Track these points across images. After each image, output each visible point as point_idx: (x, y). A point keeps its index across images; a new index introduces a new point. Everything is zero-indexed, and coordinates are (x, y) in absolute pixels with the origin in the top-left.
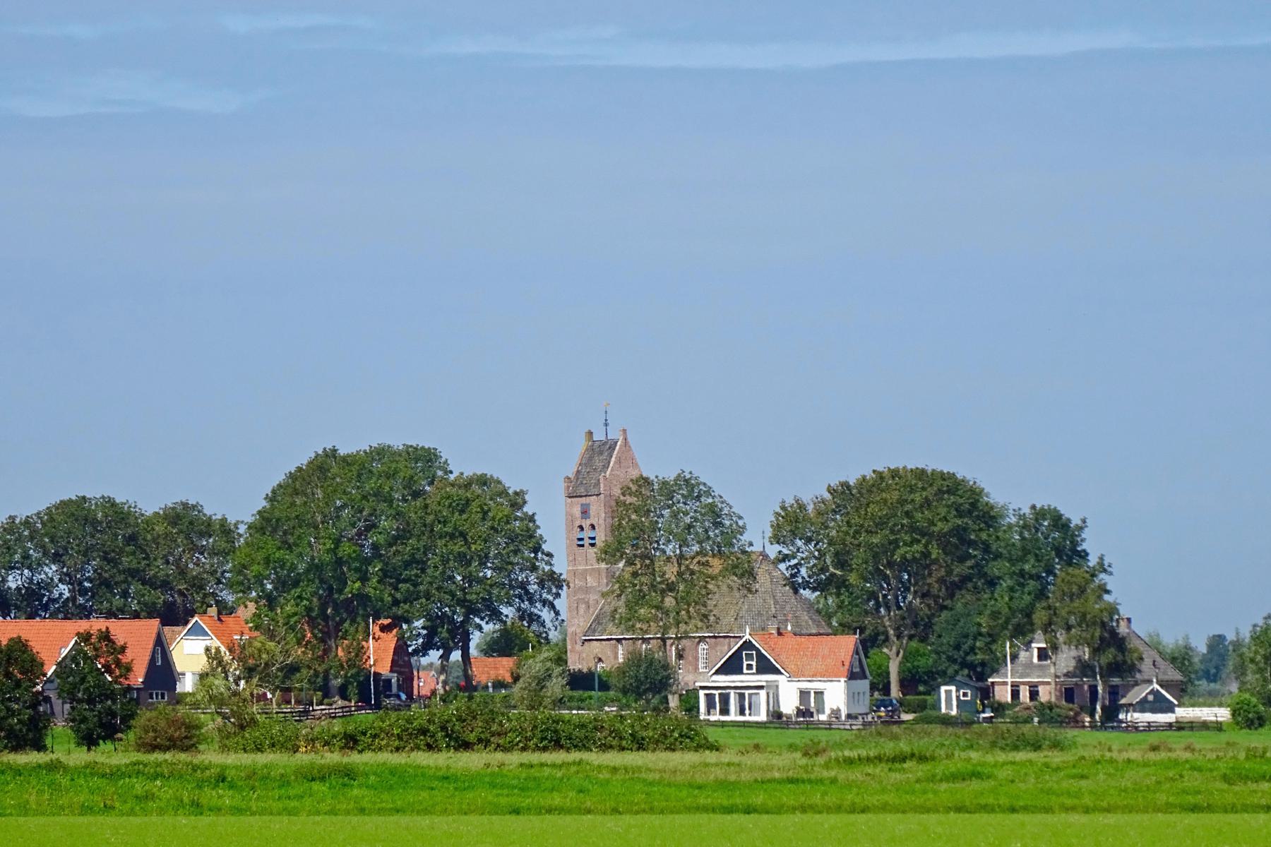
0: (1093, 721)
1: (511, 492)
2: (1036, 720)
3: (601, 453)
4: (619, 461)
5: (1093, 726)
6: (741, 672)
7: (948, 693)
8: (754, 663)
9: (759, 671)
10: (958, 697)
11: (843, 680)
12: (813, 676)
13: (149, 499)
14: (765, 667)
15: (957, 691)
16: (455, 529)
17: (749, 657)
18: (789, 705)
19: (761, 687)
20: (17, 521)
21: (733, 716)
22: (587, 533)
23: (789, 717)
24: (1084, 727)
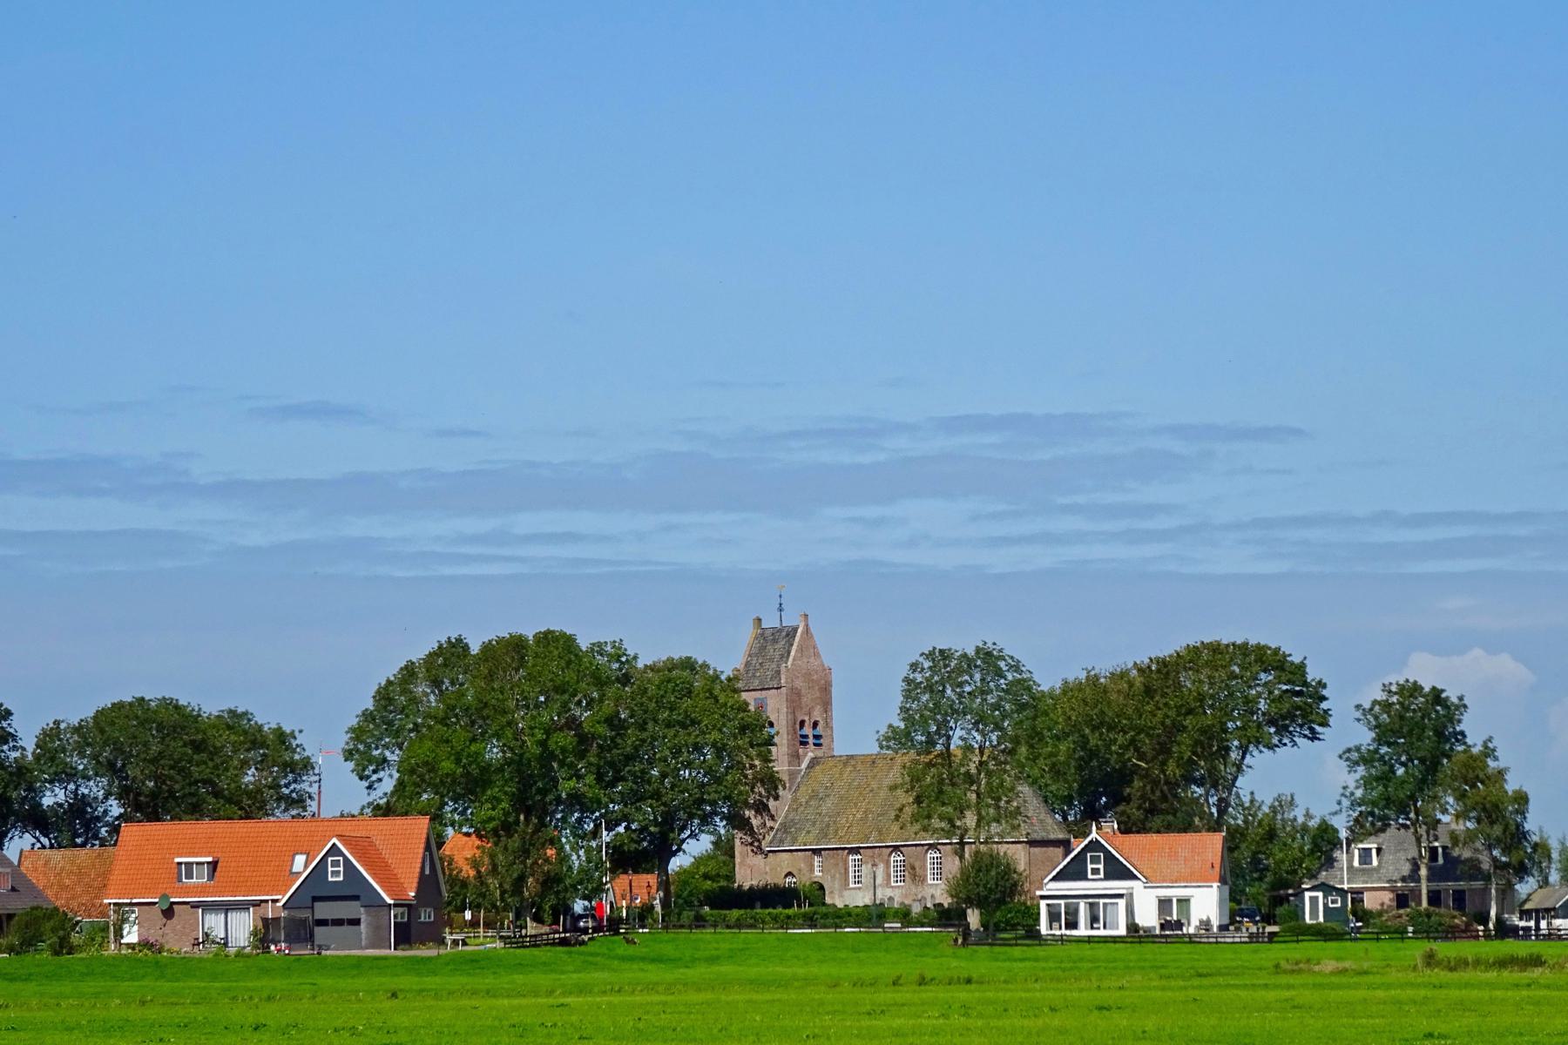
0: (1487, 930)
1: (723, 677)
2: (1410, 929)
3: (775, 641)
4: (801, 649)
5: (1487, 936)
6: (1085, 878)
7: (1314, 900)
8: (1101, 866)
9: (1108, 877)
10: (1325, 905)
11: (1215, 885)
12: (1175, 880)
13: (210, 704)
14: (1117, 871)
15: (1325, 897)
16: (687, 716)
17: (1095, 860)
18: (1148, 917)
19: (1120, 896)
20: (63, 726)
21: (1083, 931)
22: (808, 730)
23: (1146, 930)
24: (1477, 937)
